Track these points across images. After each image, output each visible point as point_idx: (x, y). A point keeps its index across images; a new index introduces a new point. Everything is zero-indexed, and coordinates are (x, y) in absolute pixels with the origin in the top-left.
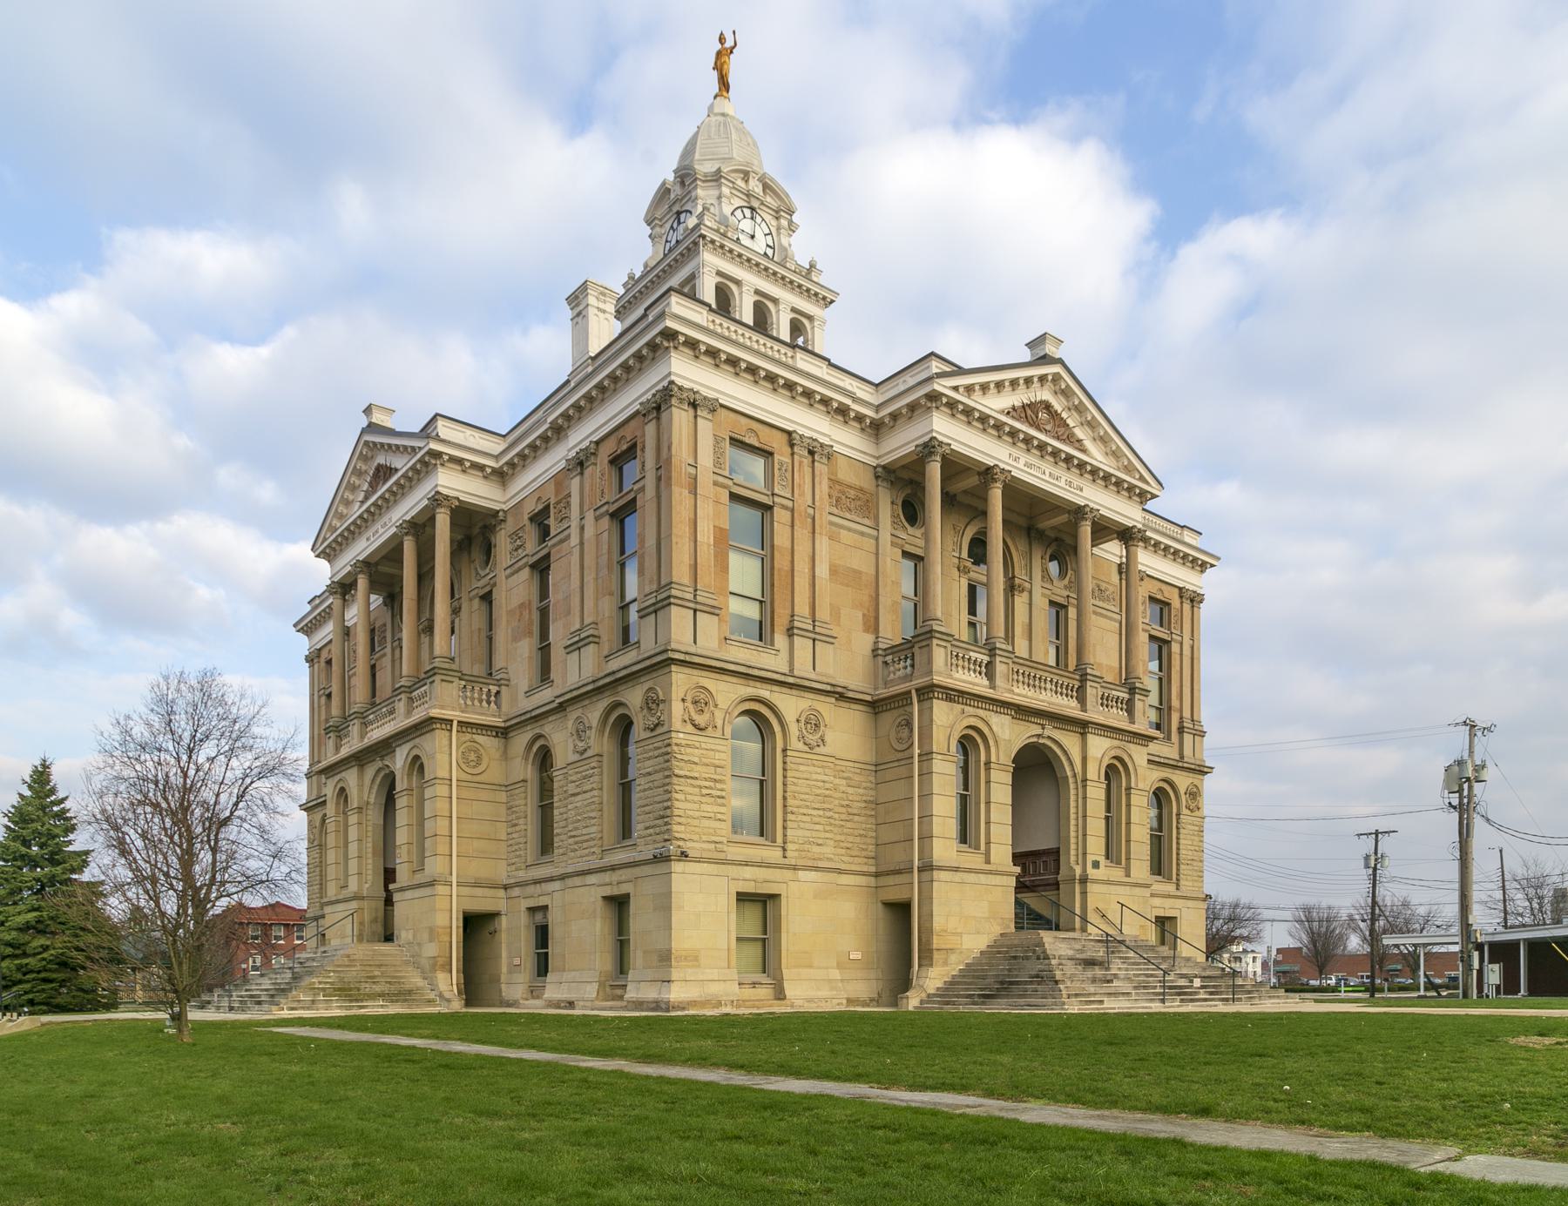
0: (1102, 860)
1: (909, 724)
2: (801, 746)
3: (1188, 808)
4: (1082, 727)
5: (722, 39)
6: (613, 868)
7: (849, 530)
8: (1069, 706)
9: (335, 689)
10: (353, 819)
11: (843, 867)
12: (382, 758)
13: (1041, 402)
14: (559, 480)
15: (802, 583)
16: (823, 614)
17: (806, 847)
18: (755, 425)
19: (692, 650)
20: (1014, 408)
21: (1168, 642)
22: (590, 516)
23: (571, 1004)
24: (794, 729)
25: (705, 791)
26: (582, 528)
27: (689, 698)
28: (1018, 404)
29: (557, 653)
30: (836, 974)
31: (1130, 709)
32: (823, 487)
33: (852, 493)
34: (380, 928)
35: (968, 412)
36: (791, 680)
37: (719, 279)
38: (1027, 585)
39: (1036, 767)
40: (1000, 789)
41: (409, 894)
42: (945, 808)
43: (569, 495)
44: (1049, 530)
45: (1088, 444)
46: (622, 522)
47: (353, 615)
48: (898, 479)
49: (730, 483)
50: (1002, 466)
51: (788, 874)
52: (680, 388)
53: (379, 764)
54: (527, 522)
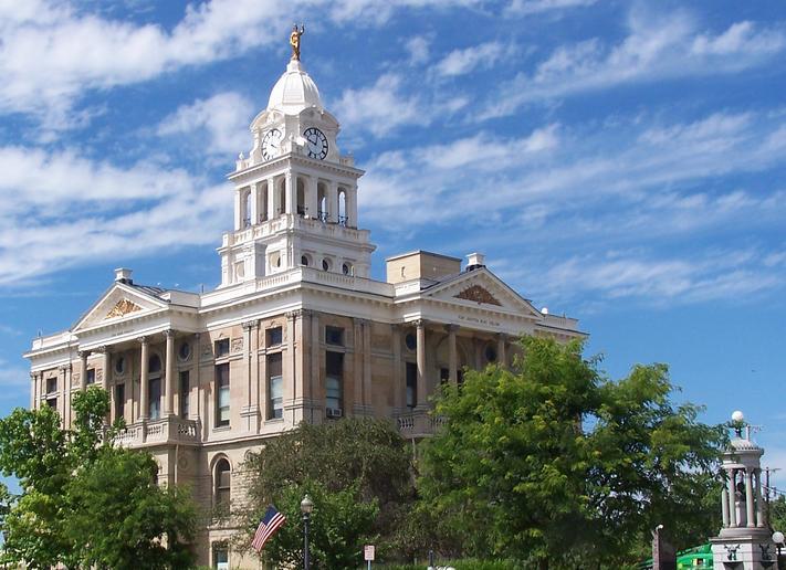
15: (358, 389)
16: (368, 401)
32: (367, 341)
45: (501, 301)
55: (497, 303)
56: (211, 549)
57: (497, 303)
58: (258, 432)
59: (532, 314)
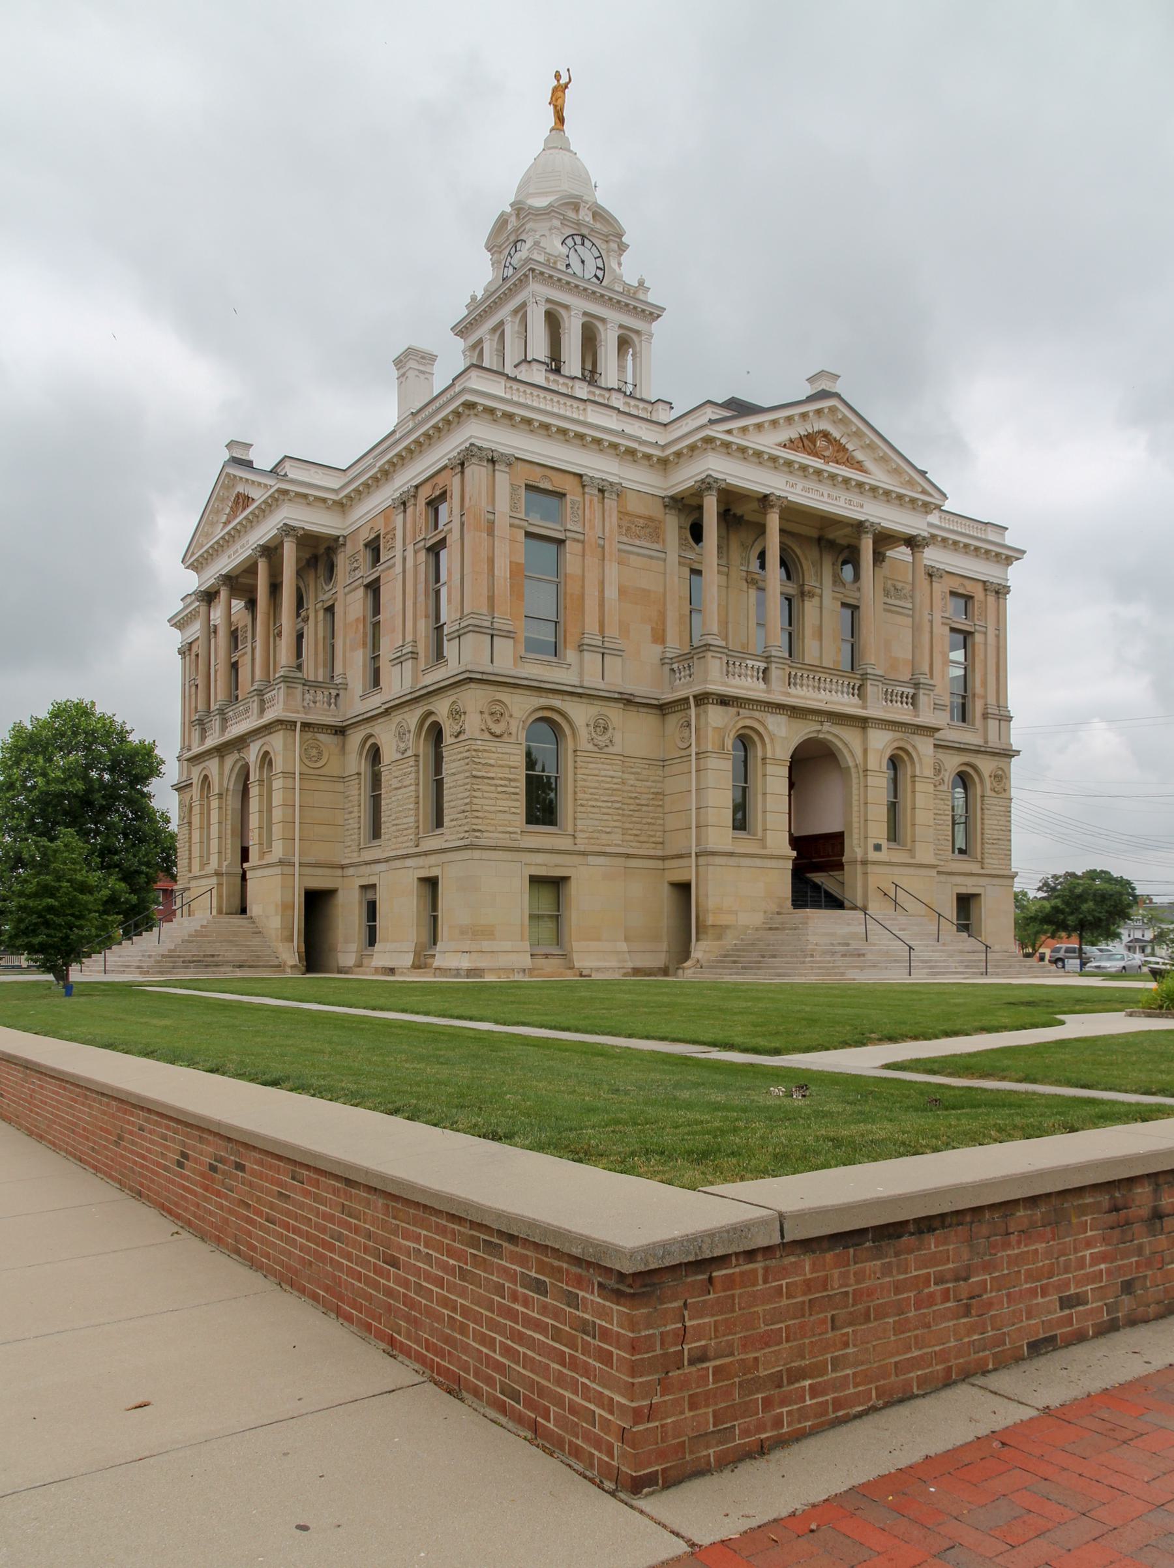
0: (884, 844)
1: (689, 725)
2: (590, 747)
3: (993, 790)
4: (863, 723)
5: (558, 76)
6: (426, 854)
7: (638, 554)
8: (846, 703)
9: (200, 681)
10: (215, 804)
11: (630, 851)
12: (239, 750)
13: (819, 432)
14: (386, 513)
15: (591, 605)
16: (612, 630)
17: (595, 835)
18: (549, 472)
19: (489, 669)
20: (791, 441)
21: (971, 633)
22: (410, 548)
23: (392, 971)
24: (583, 733)
25: (500, 789)
26: (404, 559)
27: (486, 710)
28: (794, 436)
29: (384, 664)
30: (623, 946)
31: (914, 700)
32: (613, 519)
33: (641, 522)
34: (237, 902)
35: (743, 450)
36: (580, 691)
37: (549, 306)
38: (818, 591)
39: (811, 763)
40: (773, 784)
41: (259, 873)
42: (721, 800)
43: (394, 529)
44: (830, 544)
45: (869, 464)
46: (437, 555)
47: (217, 615)
48: (684, 505)
49: (526, 524)
50: (778, 493)
51: (577, 859)
52: (480, 449)
53: (236, 756)
54: (362, 547)
55: (859, 466)
56: (507, 1363)
57: (859, 466)
58: (782, 1237)
59: (924, 492)
